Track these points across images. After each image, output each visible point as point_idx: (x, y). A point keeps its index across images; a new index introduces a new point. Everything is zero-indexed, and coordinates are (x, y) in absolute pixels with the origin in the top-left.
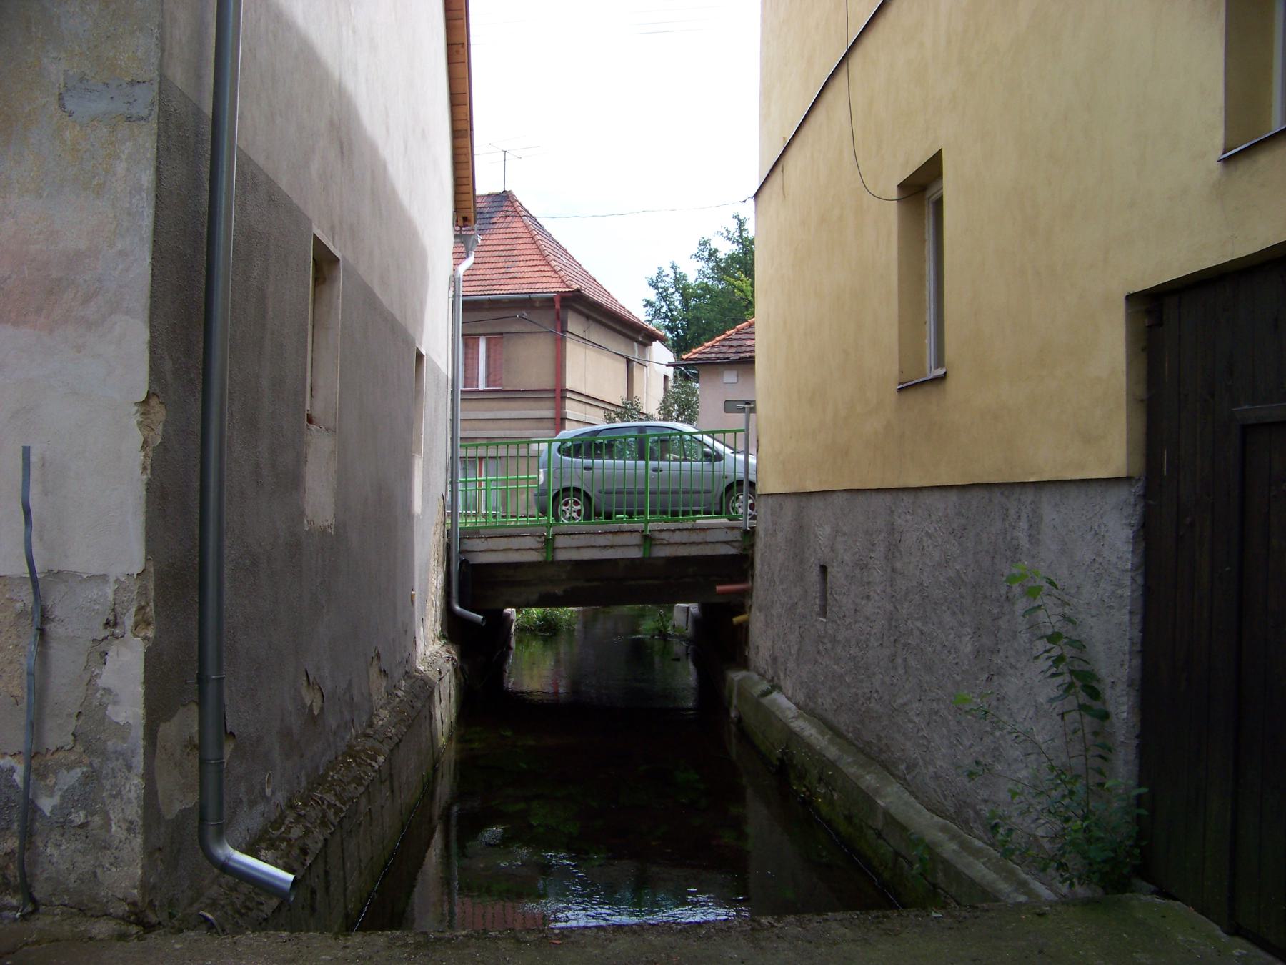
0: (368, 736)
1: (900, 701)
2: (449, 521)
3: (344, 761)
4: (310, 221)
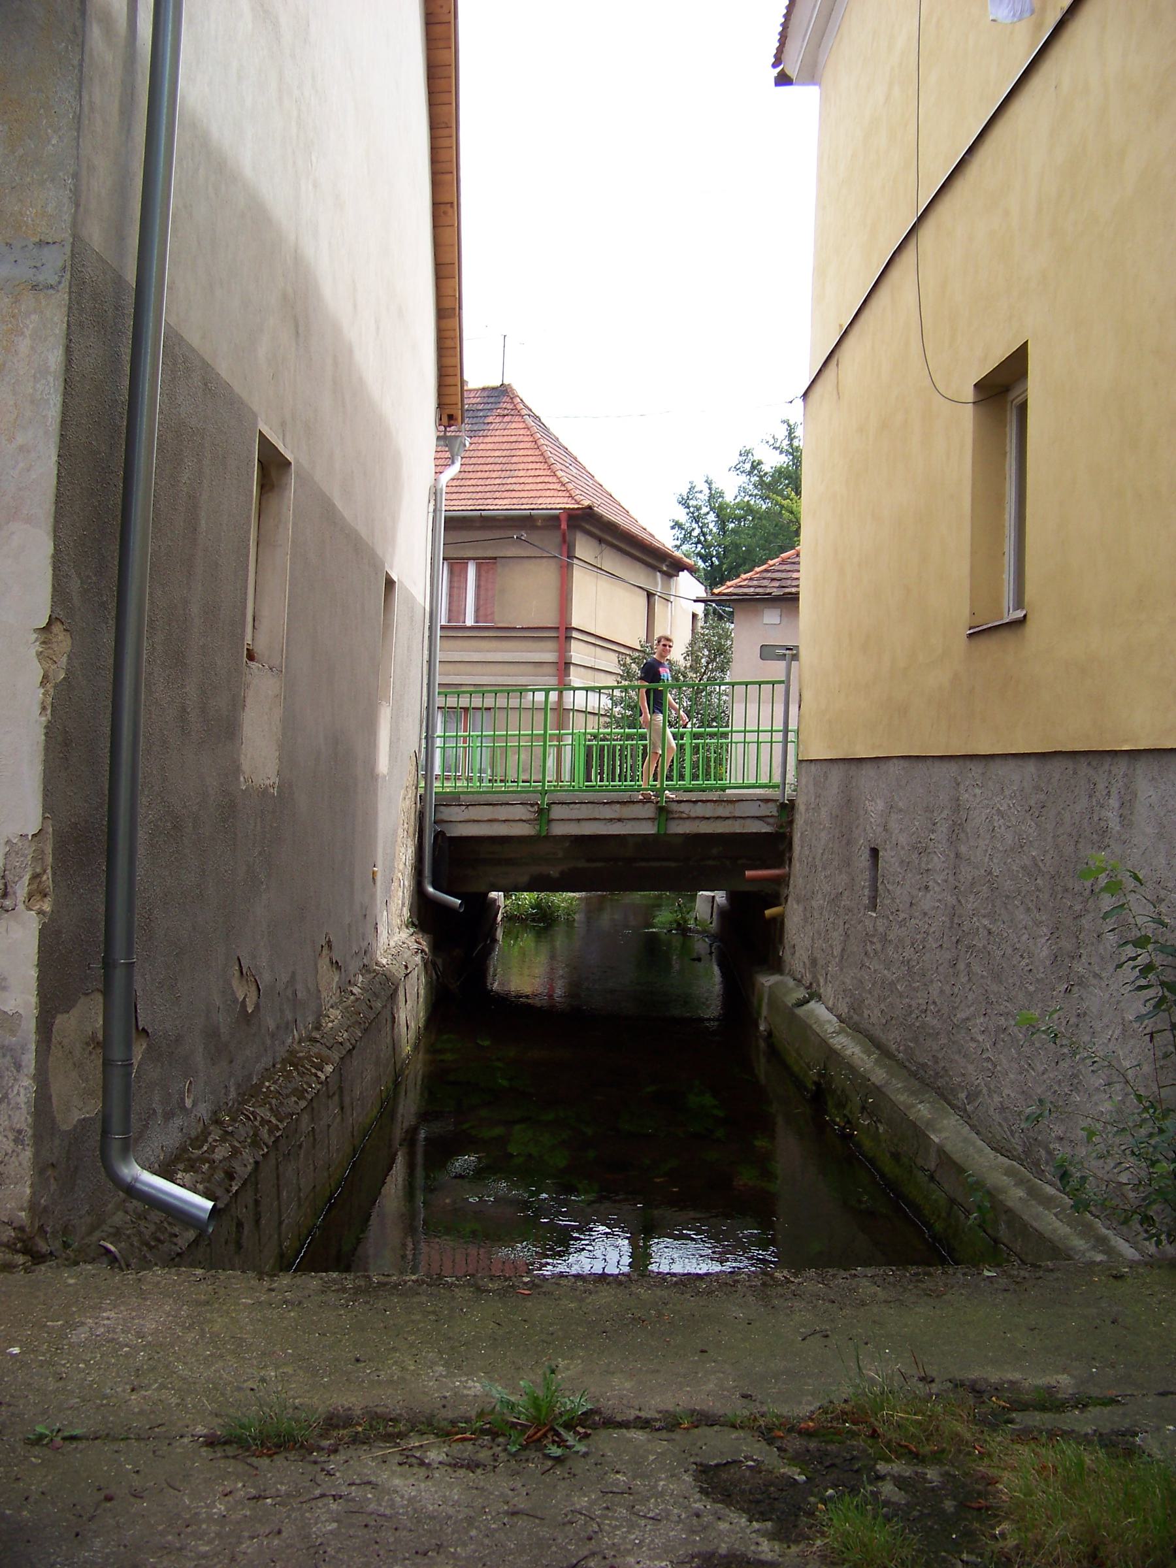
0: (315, 1040)
1: (961, 1015)
2: (422, 784)
3: (283, 1070)
4: (255, 416)
